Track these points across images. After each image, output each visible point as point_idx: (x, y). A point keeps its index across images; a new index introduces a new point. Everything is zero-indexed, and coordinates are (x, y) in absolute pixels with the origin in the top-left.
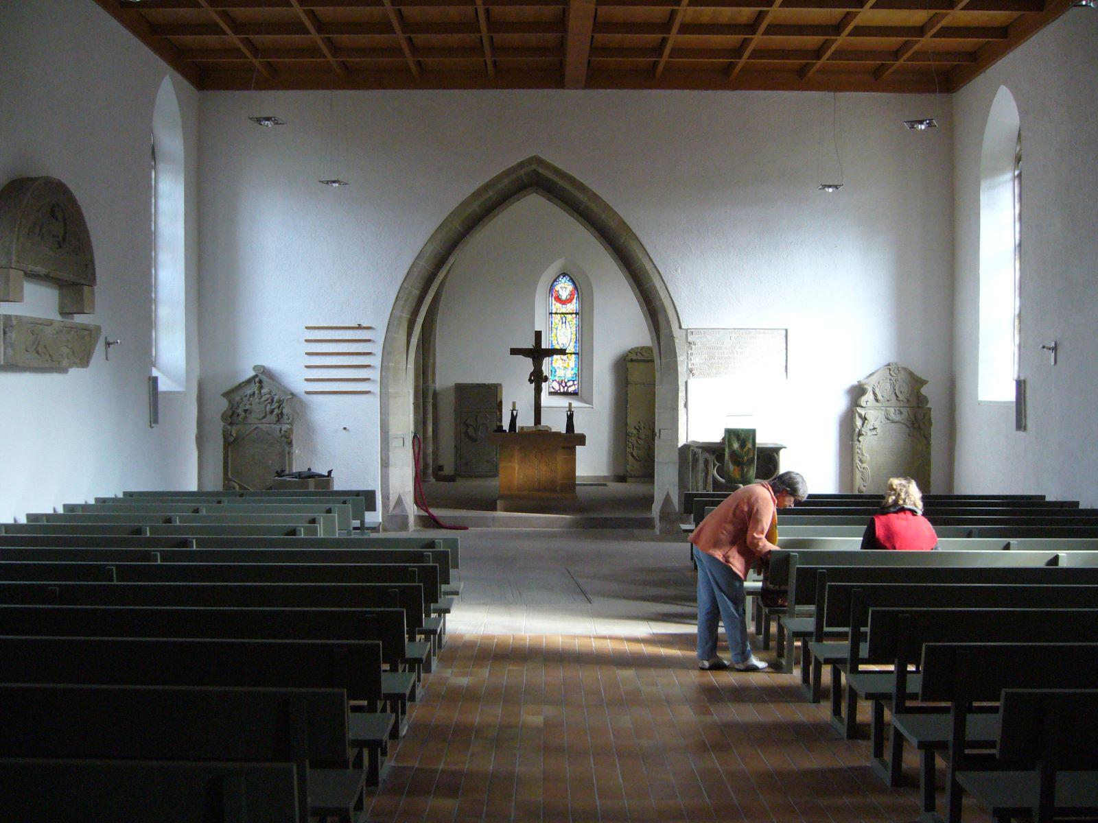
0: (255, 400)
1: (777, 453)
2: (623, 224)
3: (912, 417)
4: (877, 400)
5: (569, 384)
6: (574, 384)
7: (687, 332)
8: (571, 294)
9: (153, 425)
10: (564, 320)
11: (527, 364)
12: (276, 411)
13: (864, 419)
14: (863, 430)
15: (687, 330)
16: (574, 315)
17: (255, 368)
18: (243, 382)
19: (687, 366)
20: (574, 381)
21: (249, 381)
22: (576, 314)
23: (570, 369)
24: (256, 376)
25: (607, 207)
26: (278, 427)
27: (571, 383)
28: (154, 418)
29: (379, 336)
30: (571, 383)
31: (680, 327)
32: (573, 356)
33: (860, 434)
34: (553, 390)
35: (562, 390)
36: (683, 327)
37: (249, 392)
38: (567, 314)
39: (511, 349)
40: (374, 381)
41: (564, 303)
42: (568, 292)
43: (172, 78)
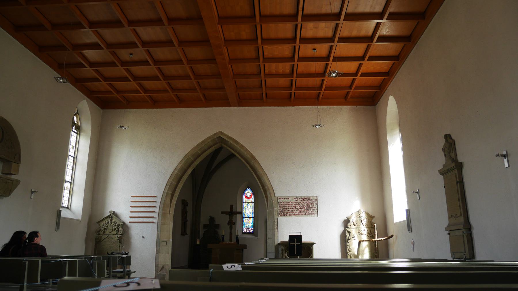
0: (109, 225)
1: (312, 247)
2: (253, 157)
3: (370, 233)
4: (354, 225)
5: (250, 229)
6: (252, 229)
7: (277, 198)
8: (251, 195)
9: (57, 230)
10: (248, 205)
11: (227, 218)
12: (116, 229)
13: (350, 233)
14: (349, 237)
15: (277, 197)
16: (252, 203)
17: (110, 212)
18: (105, 218)
19: (278, 212)
20: (252, 228)
21: (107, 217)
22: (253, 202)
23: (250, 223)
24: (110, 215)
25: (247, 150)
26: (116, 236)
27: (251, 229)
28: (58, 227)
29: (159, 200)
30: (251, 229)
31: (275, 196)
32: (252, 218)
33: (348, 239)
34: (244, 232)
35: (247, 232)
36: (276, 196)
37: (107, 221)
38: (249, 202)
39: (221, 212)
40: (155, 218)
41: (248, 198)
42: (250, 194)
43: (87, 101)
